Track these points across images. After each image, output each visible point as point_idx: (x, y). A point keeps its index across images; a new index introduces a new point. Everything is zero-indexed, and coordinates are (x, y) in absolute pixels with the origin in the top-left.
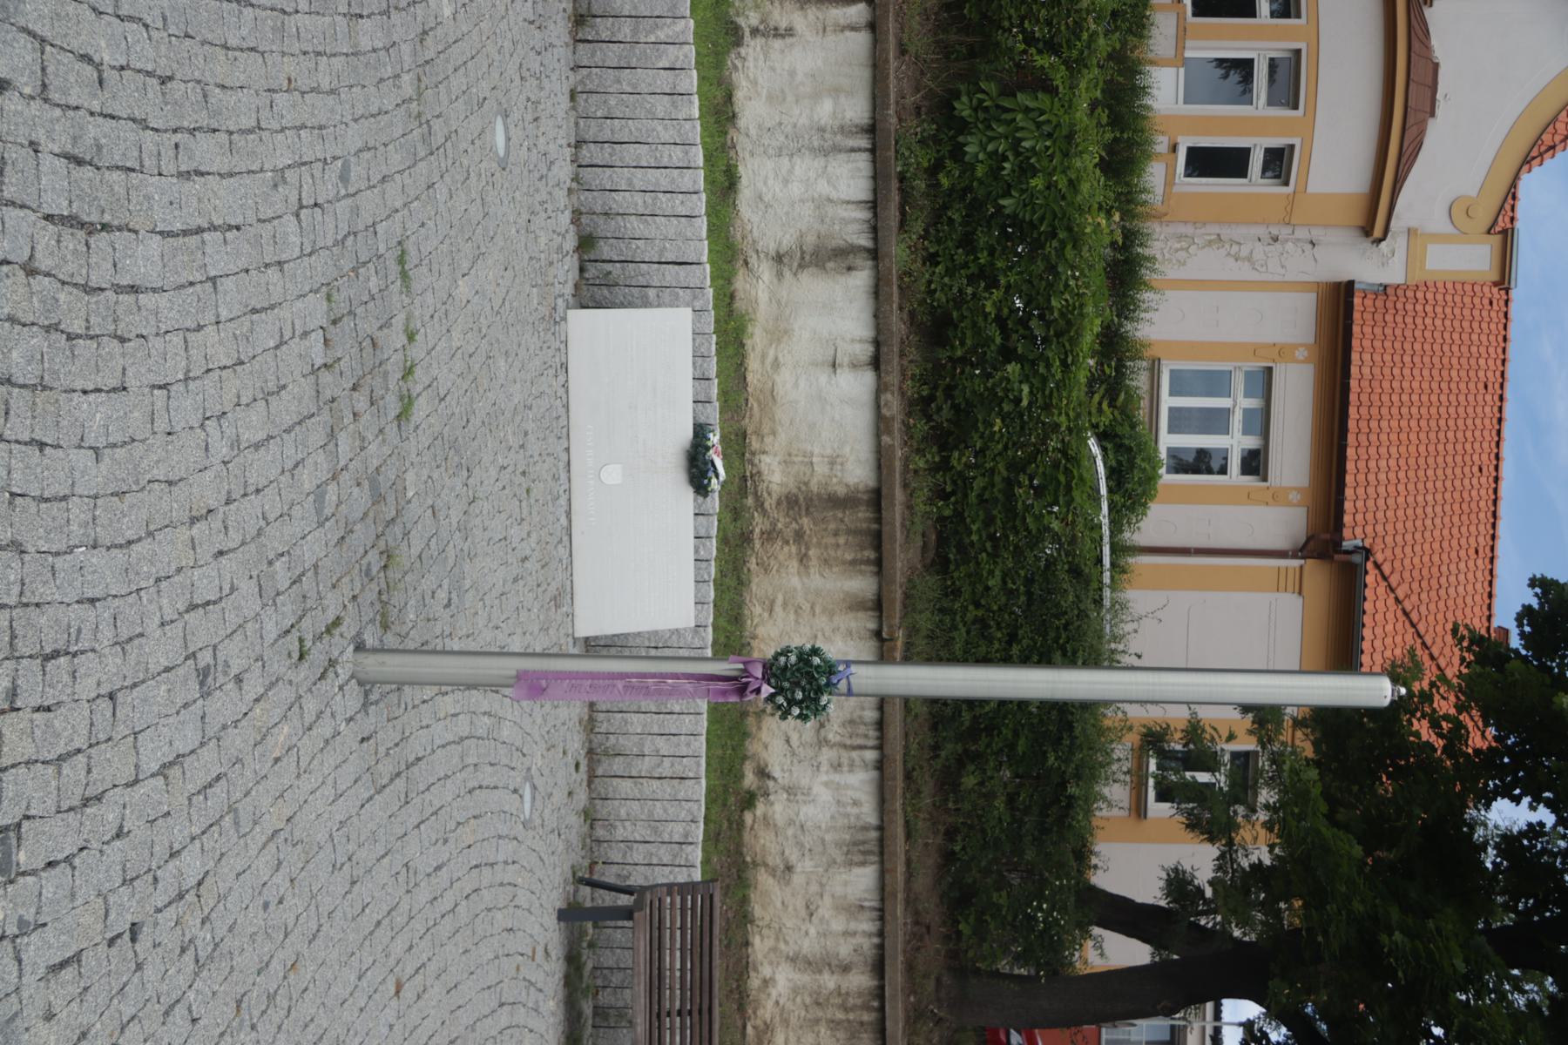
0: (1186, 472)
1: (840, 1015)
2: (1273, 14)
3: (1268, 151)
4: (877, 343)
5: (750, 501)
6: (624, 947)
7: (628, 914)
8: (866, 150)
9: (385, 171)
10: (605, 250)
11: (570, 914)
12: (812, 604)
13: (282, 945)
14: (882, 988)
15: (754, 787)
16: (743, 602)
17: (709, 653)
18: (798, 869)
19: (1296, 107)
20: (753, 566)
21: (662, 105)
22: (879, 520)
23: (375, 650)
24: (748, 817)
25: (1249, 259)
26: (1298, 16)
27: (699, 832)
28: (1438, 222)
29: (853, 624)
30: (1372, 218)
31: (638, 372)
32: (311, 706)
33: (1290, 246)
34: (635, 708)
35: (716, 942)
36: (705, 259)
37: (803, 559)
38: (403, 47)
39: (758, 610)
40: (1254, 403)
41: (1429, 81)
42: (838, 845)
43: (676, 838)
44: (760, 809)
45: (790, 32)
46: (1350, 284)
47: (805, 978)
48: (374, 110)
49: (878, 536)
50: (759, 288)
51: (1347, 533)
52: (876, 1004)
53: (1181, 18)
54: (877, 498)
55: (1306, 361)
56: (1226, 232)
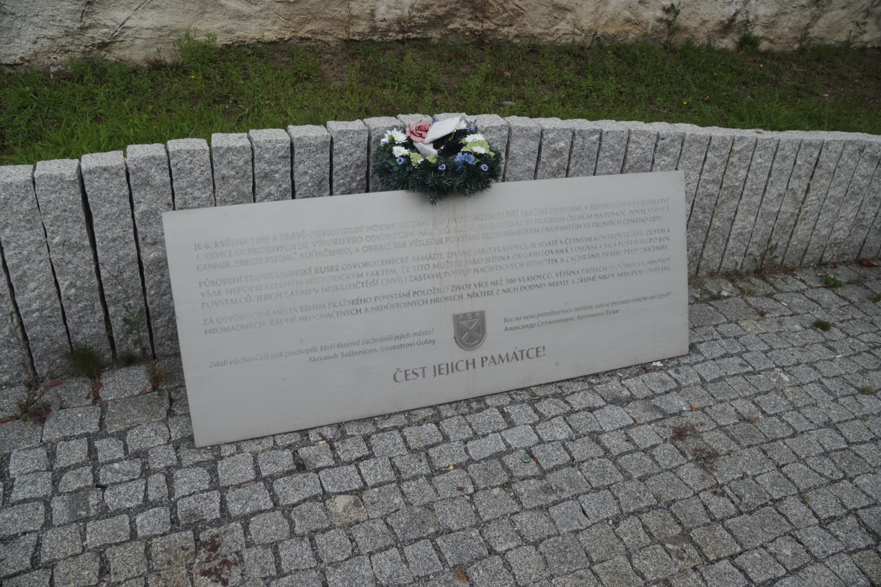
5: (435, 35)
10: (89, 331)
15: (737, 38)
16: (552, 43)
20: (513, 31)
24: (764, 46)
39: (564, 27)
44: (758, 32)
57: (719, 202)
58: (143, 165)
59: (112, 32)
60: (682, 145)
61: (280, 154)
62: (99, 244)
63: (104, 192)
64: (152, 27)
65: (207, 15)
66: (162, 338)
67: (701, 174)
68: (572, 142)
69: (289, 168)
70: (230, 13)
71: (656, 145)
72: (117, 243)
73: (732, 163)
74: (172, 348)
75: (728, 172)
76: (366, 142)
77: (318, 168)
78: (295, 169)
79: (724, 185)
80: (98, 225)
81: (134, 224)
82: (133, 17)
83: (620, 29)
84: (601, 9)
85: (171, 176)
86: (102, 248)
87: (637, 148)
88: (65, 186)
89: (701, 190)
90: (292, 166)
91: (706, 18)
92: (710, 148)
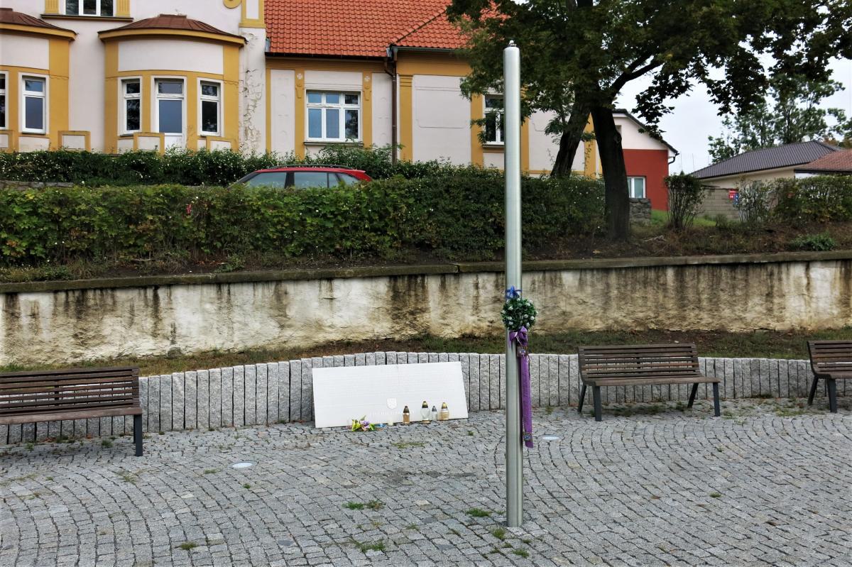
0: (357, 131)
1: (629, 288)
2: (215, 94)
3: (204, 93)
4: (321, 279)
6: (609, 391)
7: (597, 389)
8: (229, 287)
9: (278, 523)
11: (597, 415)
12: (462, 304)
13: (654, 555)
14: (616, 269)
17: (504, 355)
18: (564, 309)
19: (183, 80)
21: (215, 386)
22: (403, 276)
23: (507, 516)
25: (255, 101)
26: (139, 80)
27: (554, 356)
28: (236, 14)
29: (452, 287)
30: (234, 44)
31: (350, 394)
32: (541, 547)
33: (249, 82)
34: (497, 388)
35: (644, 346)
36: (287, 363)
37: (423, 311)
38: (215, 517)
40: (324, 99)
41: (169, 19)
42: (553, 290)
43: (556, 366)
45: (173, 326)
46: (267, 54)
47: (614, 304)
48: (250, 530)
49: (410, 276)
50: (295, 337)
51: (383, 55)
52: (624, 272)
53: (141, 135)
54: (393, 278)
55: (303, 74)
56: (242, 111)
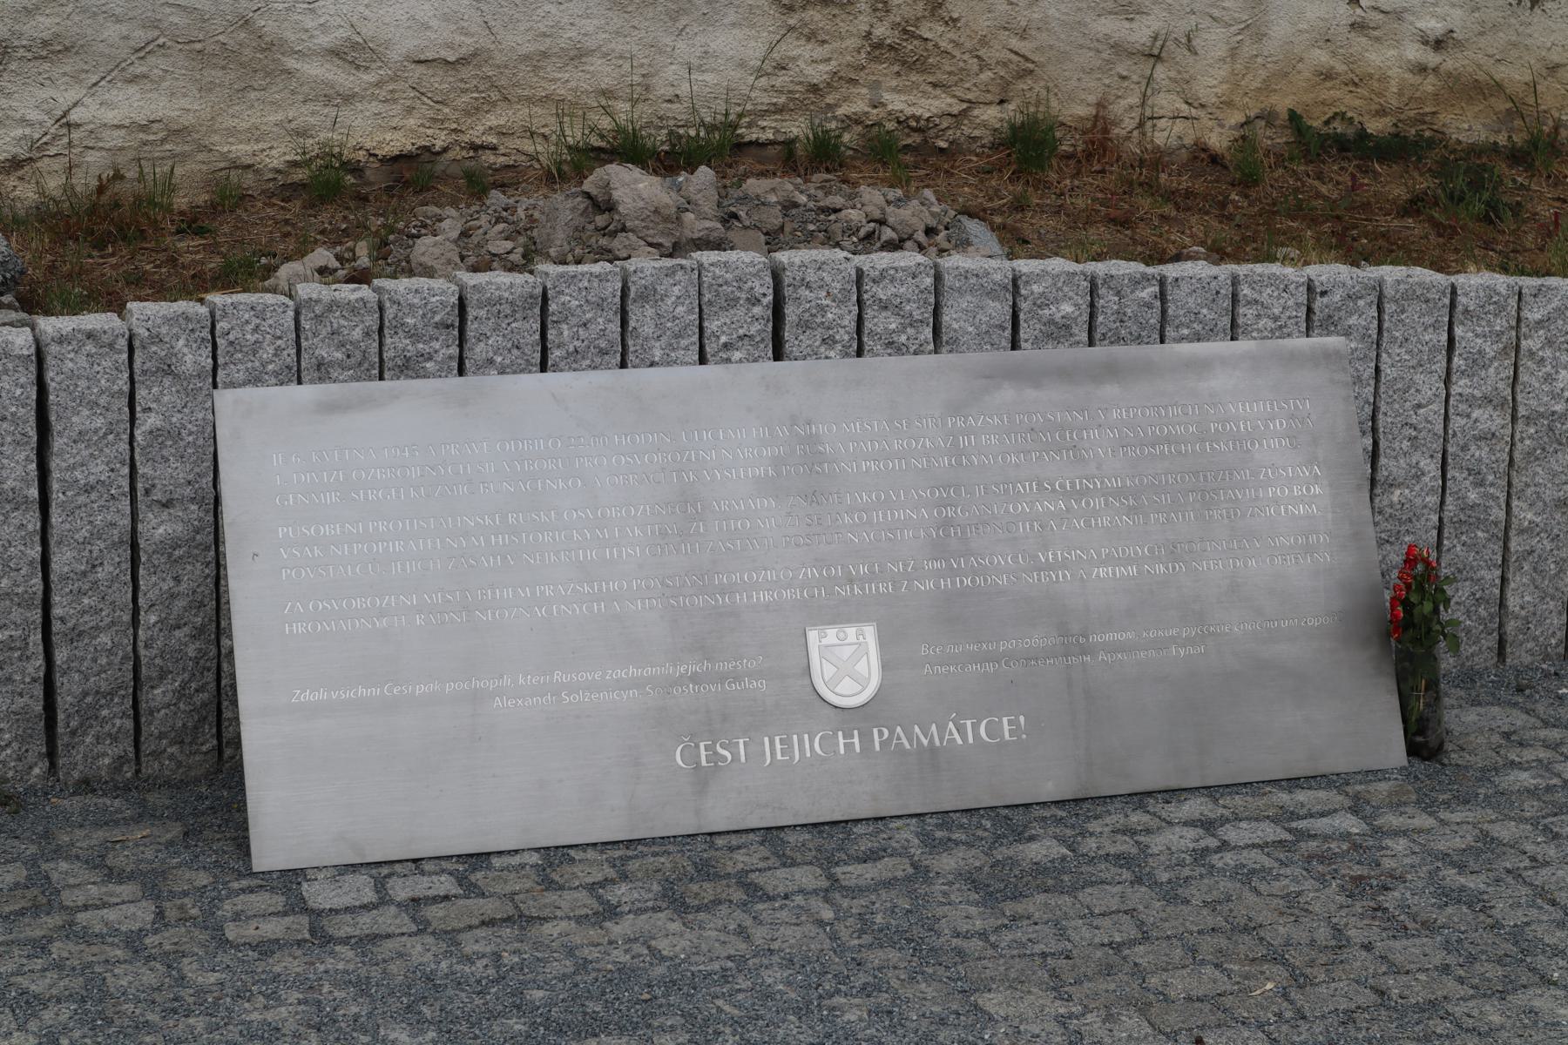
57: (1517, 456)
58: (164, 330)
59: (37, 136)
60: (1380, 310)
61: (437, 318)
62: (57, 496)
63: (83, 383)
64: (127, 122)
65: (253, 95)
66: (161, 736)
67: (1447, 382)
68: (1092, 305)
69: (454, 351)
70: (306, 89)
71: (1310, 310)
72: (94, 496)
73: (1532, 354)
74: (179, 764)
75: (1524, 377)
76: (618, 300)
77: (515, 352)
78: (467, 354)
79: (1522, 411)
80: (61, 453)
81: (132, 458)
82: (87, 101)
83: (1308, 98)
84: (1248, 50)
85: (214, 358)
86: (62, 505)
87: (1259, 316)
88: (10, 366)
89: (1457, 423)
90: (461, 346)
91: (1555, 57)
92: (1458, 315)
